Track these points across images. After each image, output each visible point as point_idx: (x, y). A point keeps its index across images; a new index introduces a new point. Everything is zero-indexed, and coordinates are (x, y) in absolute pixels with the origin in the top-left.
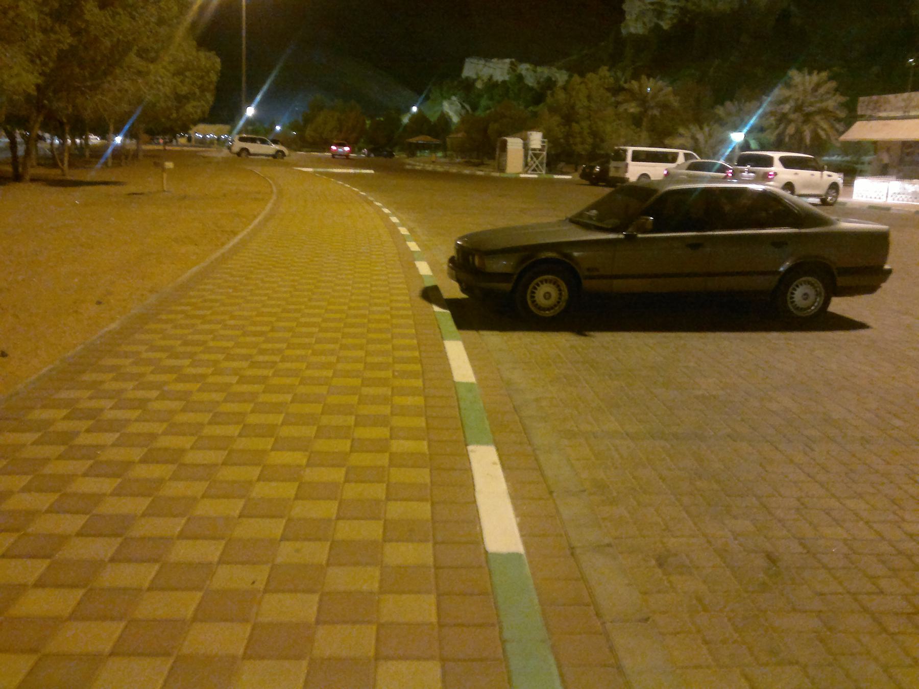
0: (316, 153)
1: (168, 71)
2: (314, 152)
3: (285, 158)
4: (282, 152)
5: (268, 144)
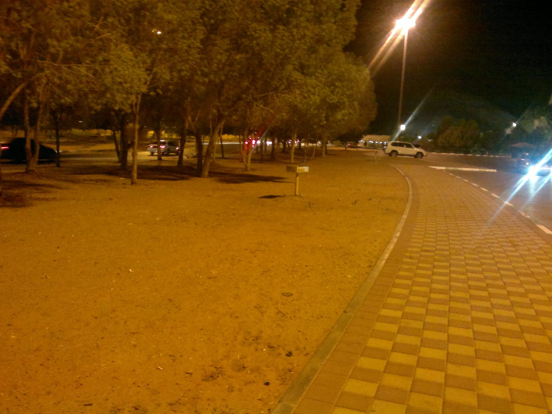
0: (443, 153)
1: (320, 82)
2: (443, 152)
3: (423, 157)
4: (421, 153)
5: (412, 148)
